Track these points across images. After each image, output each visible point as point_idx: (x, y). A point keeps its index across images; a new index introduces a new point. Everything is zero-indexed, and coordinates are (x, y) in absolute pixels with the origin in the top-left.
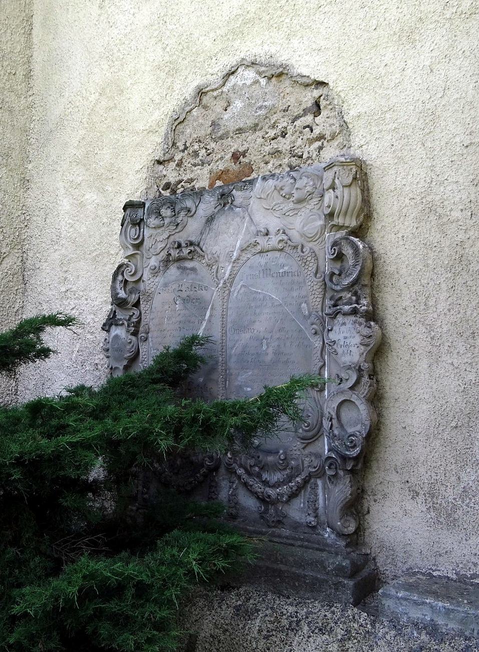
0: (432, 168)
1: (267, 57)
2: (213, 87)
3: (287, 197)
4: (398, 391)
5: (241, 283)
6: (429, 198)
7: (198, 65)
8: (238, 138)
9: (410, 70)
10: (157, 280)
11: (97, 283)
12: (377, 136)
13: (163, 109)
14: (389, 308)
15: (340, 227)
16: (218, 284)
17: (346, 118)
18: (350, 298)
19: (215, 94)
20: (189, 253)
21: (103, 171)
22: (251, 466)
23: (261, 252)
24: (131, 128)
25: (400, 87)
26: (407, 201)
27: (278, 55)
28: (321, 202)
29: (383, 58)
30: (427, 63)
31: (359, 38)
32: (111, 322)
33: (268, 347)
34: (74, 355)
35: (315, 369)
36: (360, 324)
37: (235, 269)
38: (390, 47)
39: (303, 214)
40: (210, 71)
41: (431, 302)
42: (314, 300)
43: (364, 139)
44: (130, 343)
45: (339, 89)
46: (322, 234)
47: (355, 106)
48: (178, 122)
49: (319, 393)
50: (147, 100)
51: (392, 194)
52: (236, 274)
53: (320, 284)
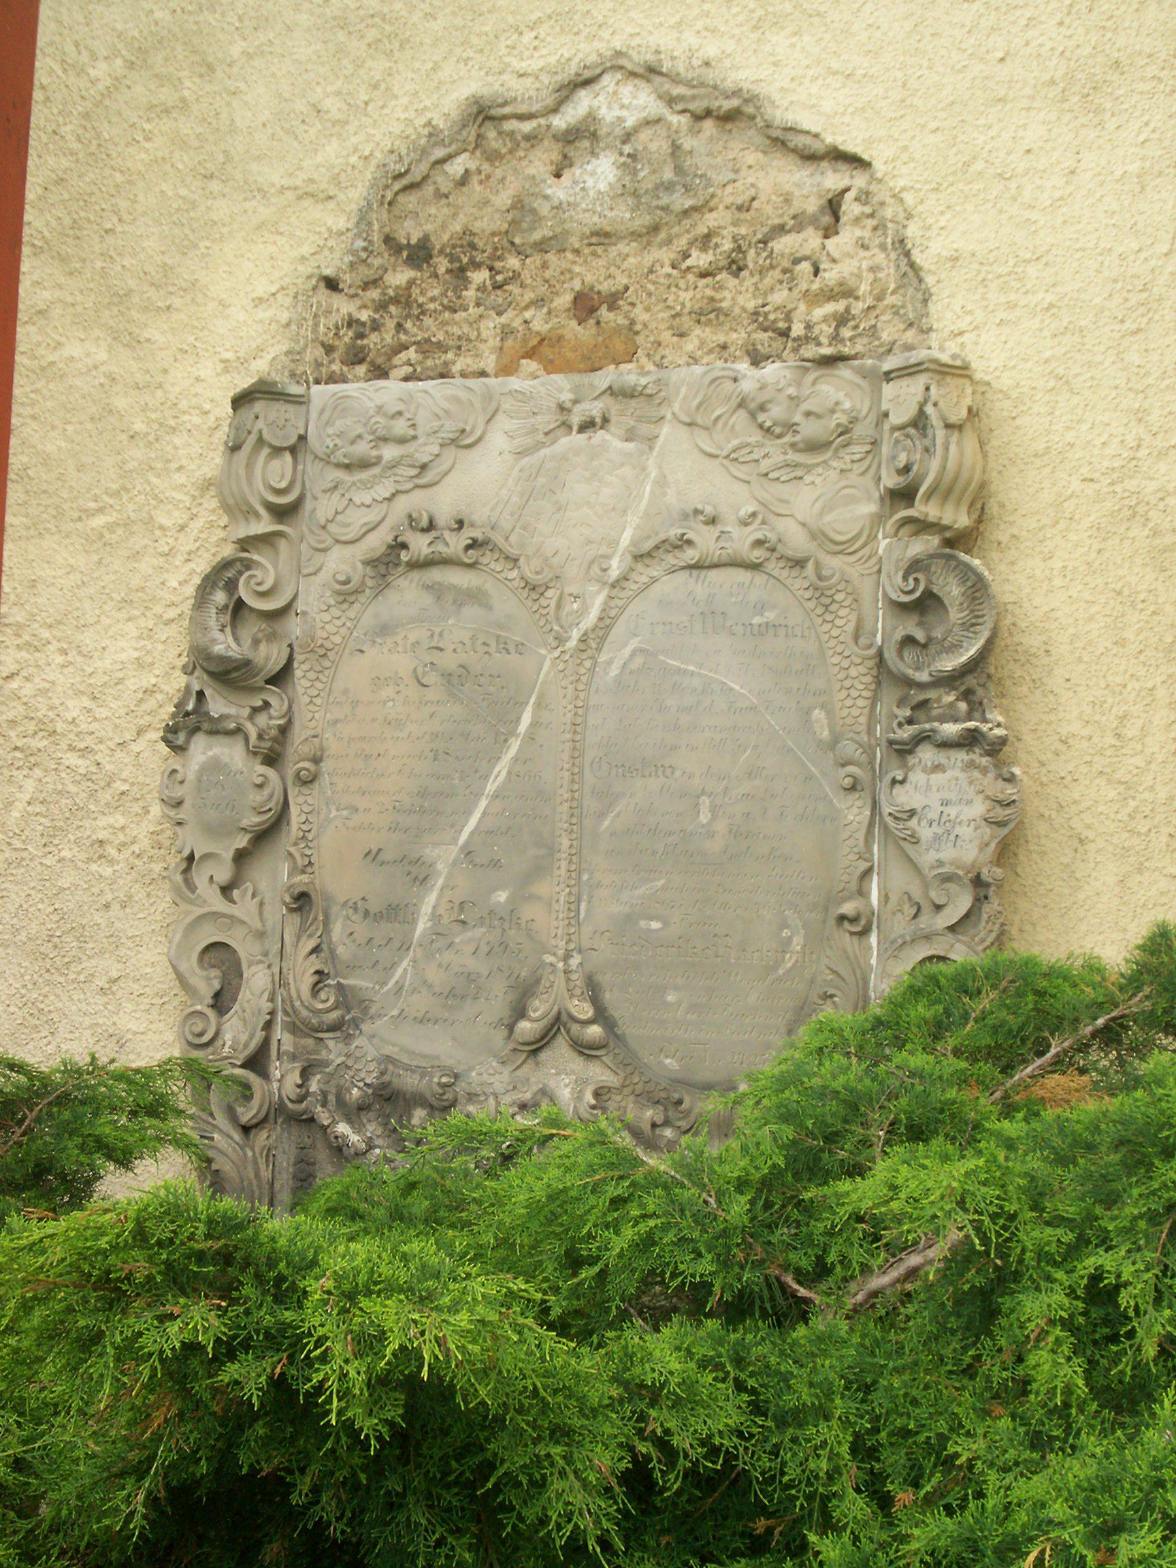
0: (1140, 416)
1: (696, 63)
2: (523, 109)
3: (778, 430)
4: (1040, 938)
5: (634, 643)
6: (1131, 485)
7: (474, 40)
8: (594, 254)
9: (1090, 174)
10: (352, 614)
11: (106, 608)
12: (1001, 315)
13: (354, 140)
14: (1025, 737)
15: (922, 526)
16: (561, 641)
17: (917, 257)
18: (951, 705)
19: (527, 127)
20: (468, 547)
21: (132, 284)
22: (654, 1125)
23: (697, 566)
24: (239, 176)
25: (1064, 209)
26: (1076, 485)
27: (727, 63)
28: (870, 457)
29: (1021, 133)
30: (1134, 167)
31: (959, 71)
32: (188, 724)
33: (714, 818)
34: (16, 814)
35: (845, 878)
36: (984, 771)
37: (613, 603)
38: (1040, 110)
39: (818, 480)
40: (517, 65)
41: (1131, 731)
42: (848, 702)
43: (969, 318)
44: (260, 786)
45: (901, 183)
46: (872, 538)
47: (944, 233)
48: (402, 183)
49: (855, 939)
50: (300, 106)
51: (1038, 462)
52: (615, 619)
53: (871, 663)
